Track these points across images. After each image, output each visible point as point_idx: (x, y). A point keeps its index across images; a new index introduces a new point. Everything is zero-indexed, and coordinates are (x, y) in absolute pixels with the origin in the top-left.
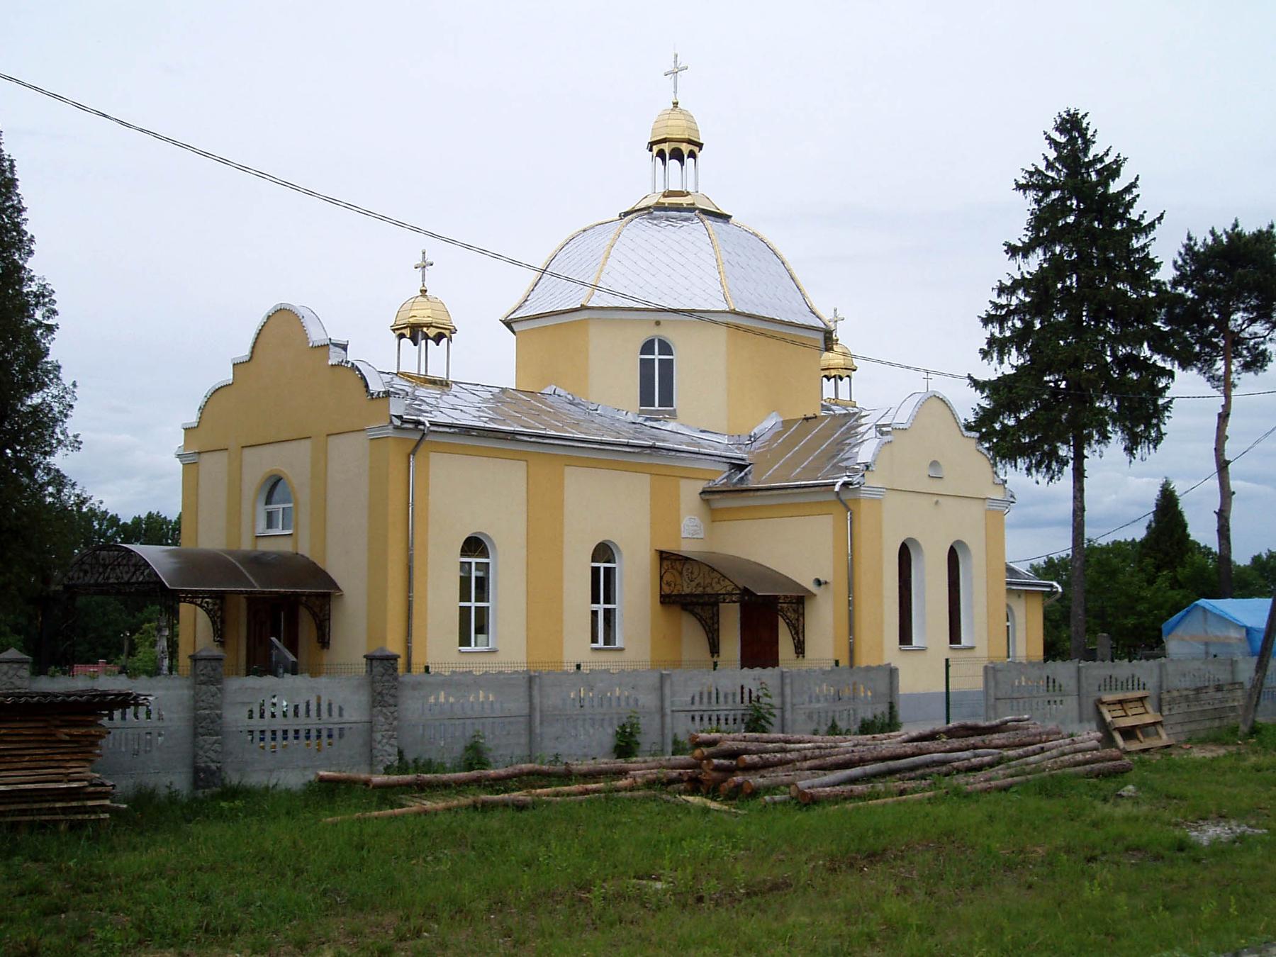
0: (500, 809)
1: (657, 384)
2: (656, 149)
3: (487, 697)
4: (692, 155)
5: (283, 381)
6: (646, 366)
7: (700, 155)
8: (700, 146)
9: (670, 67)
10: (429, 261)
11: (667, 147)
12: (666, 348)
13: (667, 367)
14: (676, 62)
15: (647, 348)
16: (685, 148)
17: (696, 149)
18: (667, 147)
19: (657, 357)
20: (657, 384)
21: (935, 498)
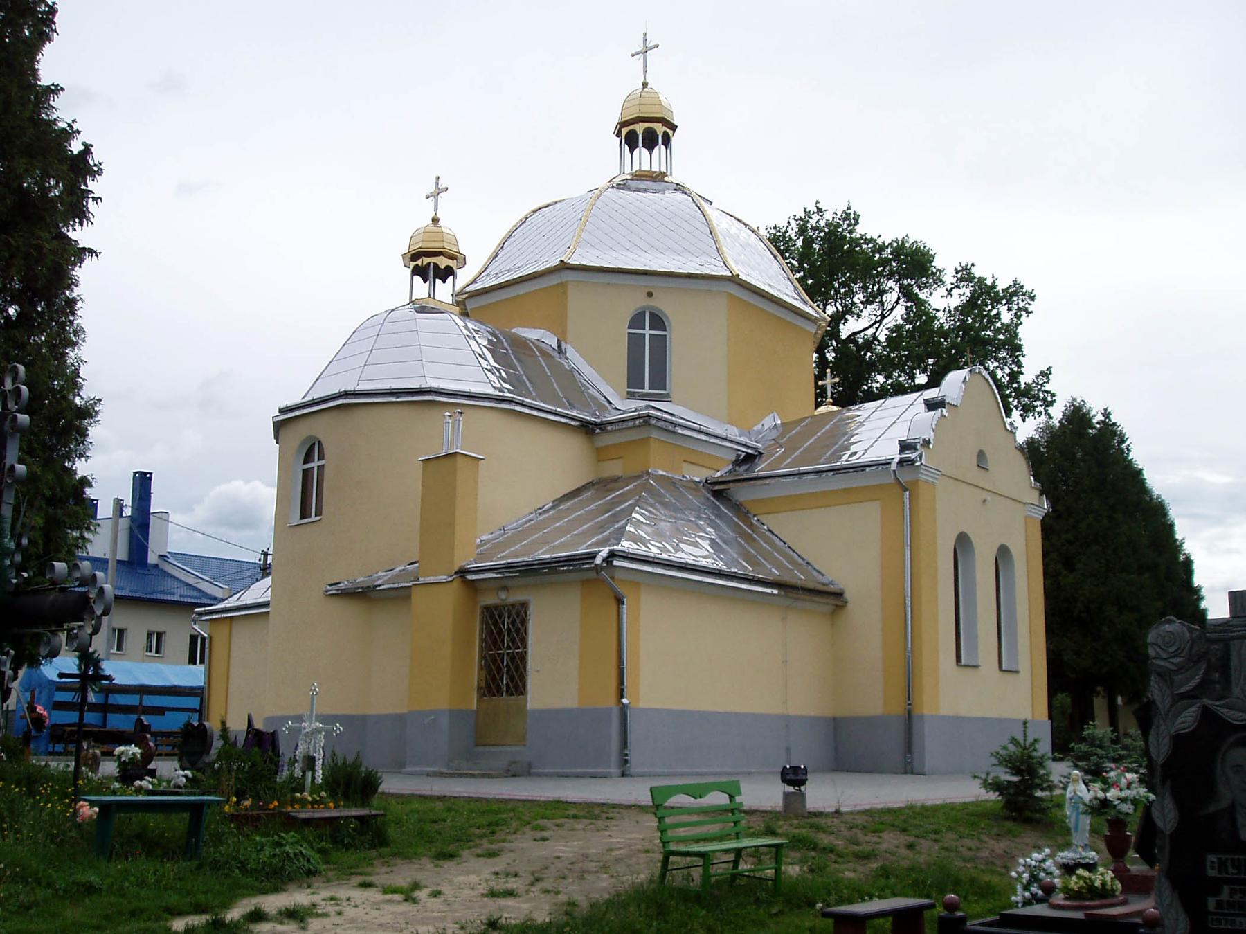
0: (152, 730)
1: (648, 364)
2: (624, 131)
3: (40, 183)
4: (667, 141)
5: (270, 720)
6: (635, 343)
7: (675, 139)
8: (674, 128)
9: (431, 189)
10: (442, 186)
11: (640, 128)
12: (658, 321)
13: (660, 345)
14: (437, 184)
15: (637, 321)
16: (660, 129)
17: (670, 132)
18: (640, 128)
19: (647, 332)
20: (648, 364)
21: (984, 495)
